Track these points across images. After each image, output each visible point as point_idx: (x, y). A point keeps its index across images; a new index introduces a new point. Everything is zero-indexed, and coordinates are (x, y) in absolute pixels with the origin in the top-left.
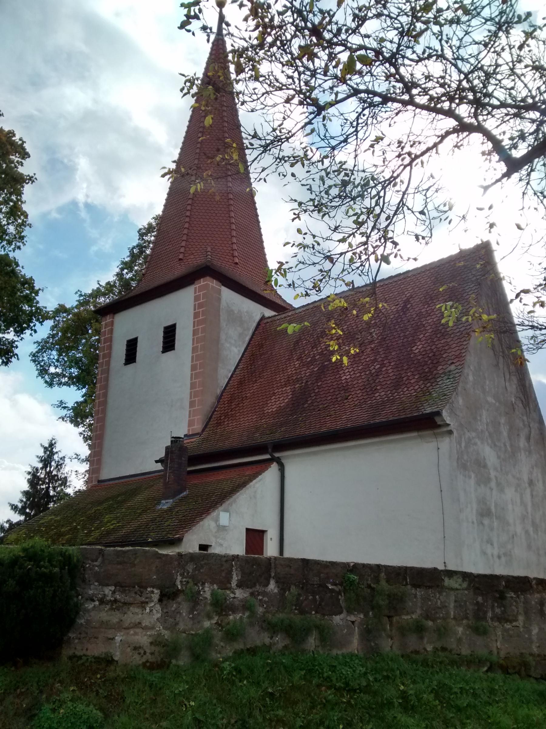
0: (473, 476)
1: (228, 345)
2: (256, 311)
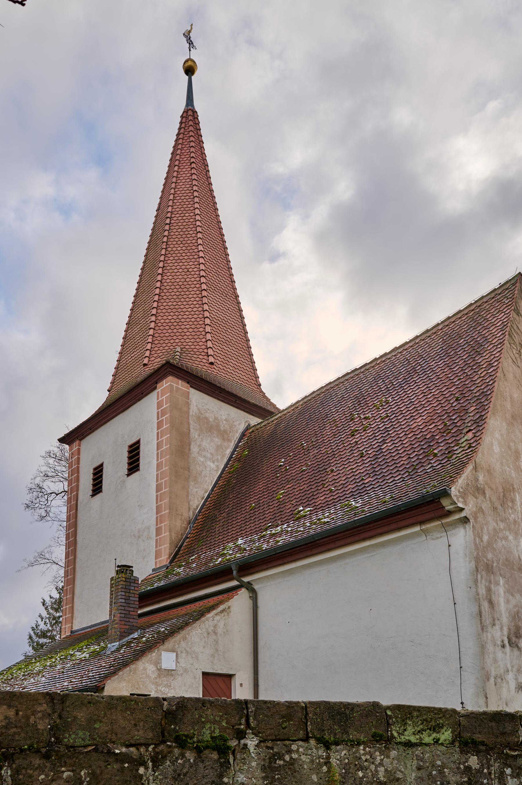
0: (502, 582)
1: (202, 460)
2: (240, 421)
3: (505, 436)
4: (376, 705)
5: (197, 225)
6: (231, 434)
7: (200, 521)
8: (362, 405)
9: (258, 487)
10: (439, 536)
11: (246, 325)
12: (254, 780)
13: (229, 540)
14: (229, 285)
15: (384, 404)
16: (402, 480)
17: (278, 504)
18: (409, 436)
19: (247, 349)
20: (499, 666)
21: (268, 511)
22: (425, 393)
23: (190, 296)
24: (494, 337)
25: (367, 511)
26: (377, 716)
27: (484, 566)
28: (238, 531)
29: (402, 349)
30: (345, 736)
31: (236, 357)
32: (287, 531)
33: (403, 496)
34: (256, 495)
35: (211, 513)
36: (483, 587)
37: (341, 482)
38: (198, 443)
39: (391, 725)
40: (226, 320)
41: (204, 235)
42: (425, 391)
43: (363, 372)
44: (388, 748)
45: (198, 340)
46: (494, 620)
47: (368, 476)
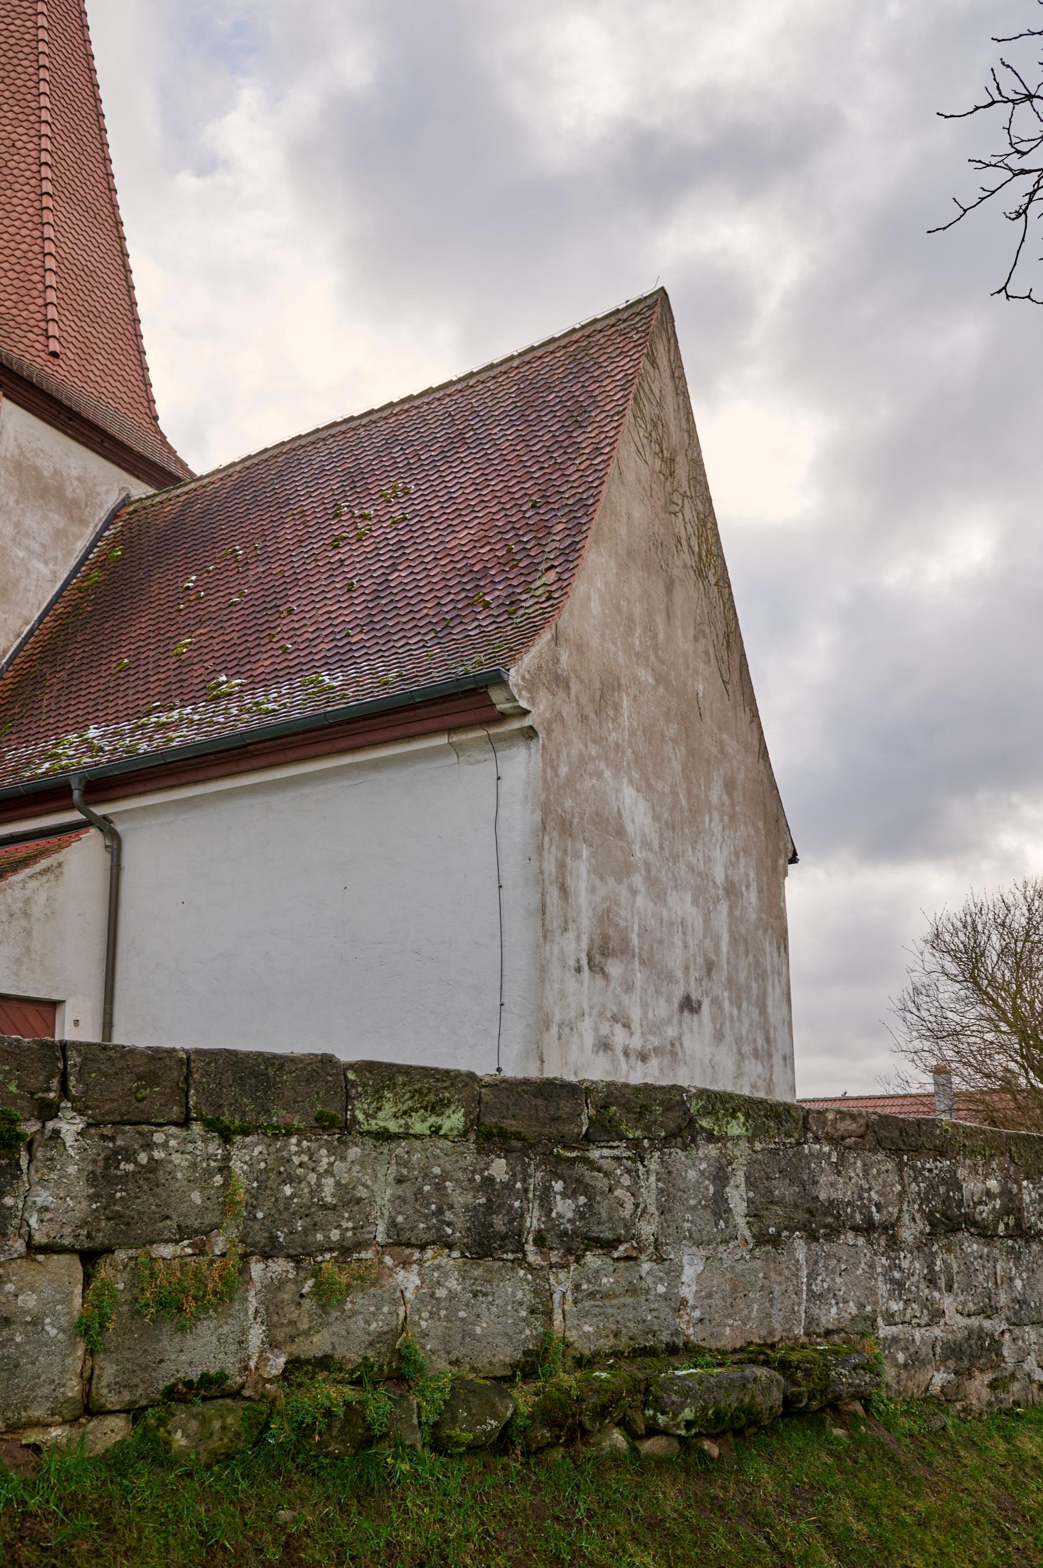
0: (585, 853)
1: (21, 554)
2: (111, 486)
3: (612, 587)
4: (327, 1060)
5: (40, 50)
6: (88, 509)
7: (8, 681)
8: (358, 490)
9: (137, 627)
10: (481, 757)
11: (134, 288)
12: (70, 1202)
13: (69, 728)
14: (104, 196)
15: (400, 494)
16: (421, 644)
17: (177, 664)
18: (442, 563)
19: (134, 338)
20: (568, 1006)
21: (155, 678)
22: (478, 484)
23: (15, 201)
24: (608, 400)
25: (353, 697)
26: (327, 1082)
27: (557, 821)
28: (91, 710)
29: (442, 393)
30: (262, 1119)
31: (109, 351)
32: (192, 721)
33: (422, 676)
34: (132, 641)
35: (35, 669)
36: (552, 859)
37: (306, 636)
38: (15, 519)
39: (354, 1098)
40: (92, 268)
41: (55, 76)
42: (477, 481)
43: (364, 426)
44: (344, 1142)
45: (27, 299)
46: (566, 922)
47: (359, 629)
